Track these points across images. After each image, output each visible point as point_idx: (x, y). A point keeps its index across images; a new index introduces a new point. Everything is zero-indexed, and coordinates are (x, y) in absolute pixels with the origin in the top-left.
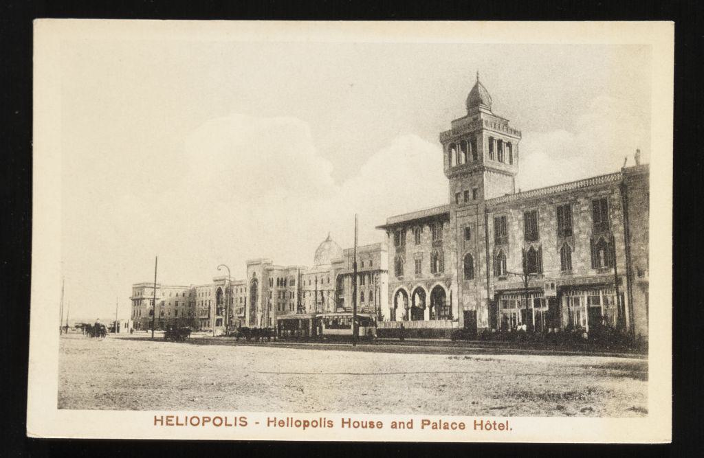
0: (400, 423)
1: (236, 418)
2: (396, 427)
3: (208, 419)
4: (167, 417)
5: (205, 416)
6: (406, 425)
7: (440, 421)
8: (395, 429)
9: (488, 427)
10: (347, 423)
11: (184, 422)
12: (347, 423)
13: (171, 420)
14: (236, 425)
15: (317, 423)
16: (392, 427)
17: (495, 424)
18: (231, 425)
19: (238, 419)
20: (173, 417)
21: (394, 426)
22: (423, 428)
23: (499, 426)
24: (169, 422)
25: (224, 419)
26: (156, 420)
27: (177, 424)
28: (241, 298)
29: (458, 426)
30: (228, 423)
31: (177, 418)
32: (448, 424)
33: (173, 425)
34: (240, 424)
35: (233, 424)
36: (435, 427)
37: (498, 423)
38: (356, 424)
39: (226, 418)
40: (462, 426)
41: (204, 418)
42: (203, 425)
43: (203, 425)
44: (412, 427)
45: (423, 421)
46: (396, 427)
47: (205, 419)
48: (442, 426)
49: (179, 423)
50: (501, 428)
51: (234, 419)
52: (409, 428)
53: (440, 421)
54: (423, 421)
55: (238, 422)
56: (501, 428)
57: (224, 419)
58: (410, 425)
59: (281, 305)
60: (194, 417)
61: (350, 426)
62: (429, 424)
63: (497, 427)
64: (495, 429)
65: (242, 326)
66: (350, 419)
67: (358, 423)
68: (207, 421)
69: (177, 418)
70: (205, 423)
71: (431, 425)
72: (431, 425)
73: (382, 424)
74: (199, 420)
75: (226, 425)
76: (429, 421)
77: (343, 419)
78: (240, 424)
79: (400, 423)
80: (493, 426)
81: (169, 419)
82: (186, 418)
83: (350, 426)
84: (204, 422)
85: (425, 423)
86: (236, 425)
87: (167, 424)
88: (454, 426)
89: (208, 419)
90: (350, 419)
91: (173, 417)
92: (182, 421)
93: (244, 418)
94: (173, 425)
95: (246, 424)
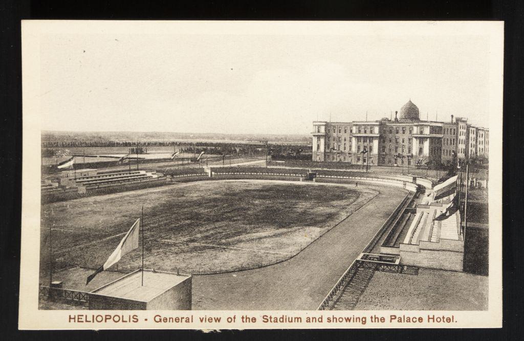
0: (313, 318)
1: (130, 316)
2: (310, 322)
3: (109, 317)
4: (79, 316)
5: (107, 314)
6: (251, 320)
7: (404, 316)
8: (409, 323)
9: (439, 320)
10: (73, 319)
11: (91, 320)
12: (73, 319)
13: (81, 319)
14: (130, 321)
15: (280, 321)
16: (307, 321)
17: (443, 318)
18: (90, 321)
19: (131, 317)
20: (82, 316)
21: (308, 320)
22: (391, 321)
23: (447, 320)
24: (80, 320)
25: (121, 318)
26: (70, 318)
27: (86, 321)
28: (447, 139)
29: (417, 320)
30: (124, 320)
31: (86, 316)
32: (277, 318)
33: (82, 322)
34: (133, 321)
35: (128, 321)
36: (400, 320)
37: (446, 317)
38: (341, 320)
39: (123, 316)
40: (420, 320)
41: (106, 316)
42: (106, 321)
43: (106, 321)
44: (322, 321)
45: (391, 316)
46: (310, 322)
47: (107, 317)
48: (406, 320)
49: (88, 320)
50: (177, 321)
51: (92, 317)
52: (319, 322)
53: (404, 316)
54: (391, 316)
55: (132, 319)
56: (177, 321)
57: (121, 318)
58: (320, 320)
59: (452, 140)
60: (155, 317)
61: (434, 321)
62: (395, 318)
63: (273, 320)
64: (444, 321)
65: (73, 168)
66: (434, 316)
67: (437, 321)
68: (394, 319)
69: (86, 316)
70: (107, 320)
71: (397, 319)
72: (397, 319)
73: (384, 319)
74: (96, 319)
75: (123, 321)
76: (110, 316)
77: (429, 316)
78: (133, 321)
79: (170, 318)
80: (442, 319)
81: (80, 317)
82: (93, 316)
83: (434, 321)
84: (106, 319)
85: (393, 317)
86: (130, 321)
87: (78, 321)
88: (414, 320)
89: (109, 317)
90: (434, 316)
91: (82, 316)
92: (126, 319)
93: (266, 316)
94: (82, 322)
95: (263, 318)
